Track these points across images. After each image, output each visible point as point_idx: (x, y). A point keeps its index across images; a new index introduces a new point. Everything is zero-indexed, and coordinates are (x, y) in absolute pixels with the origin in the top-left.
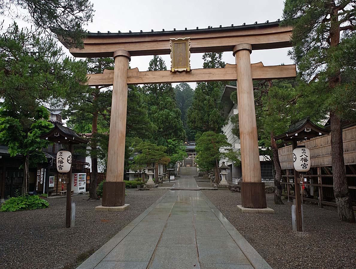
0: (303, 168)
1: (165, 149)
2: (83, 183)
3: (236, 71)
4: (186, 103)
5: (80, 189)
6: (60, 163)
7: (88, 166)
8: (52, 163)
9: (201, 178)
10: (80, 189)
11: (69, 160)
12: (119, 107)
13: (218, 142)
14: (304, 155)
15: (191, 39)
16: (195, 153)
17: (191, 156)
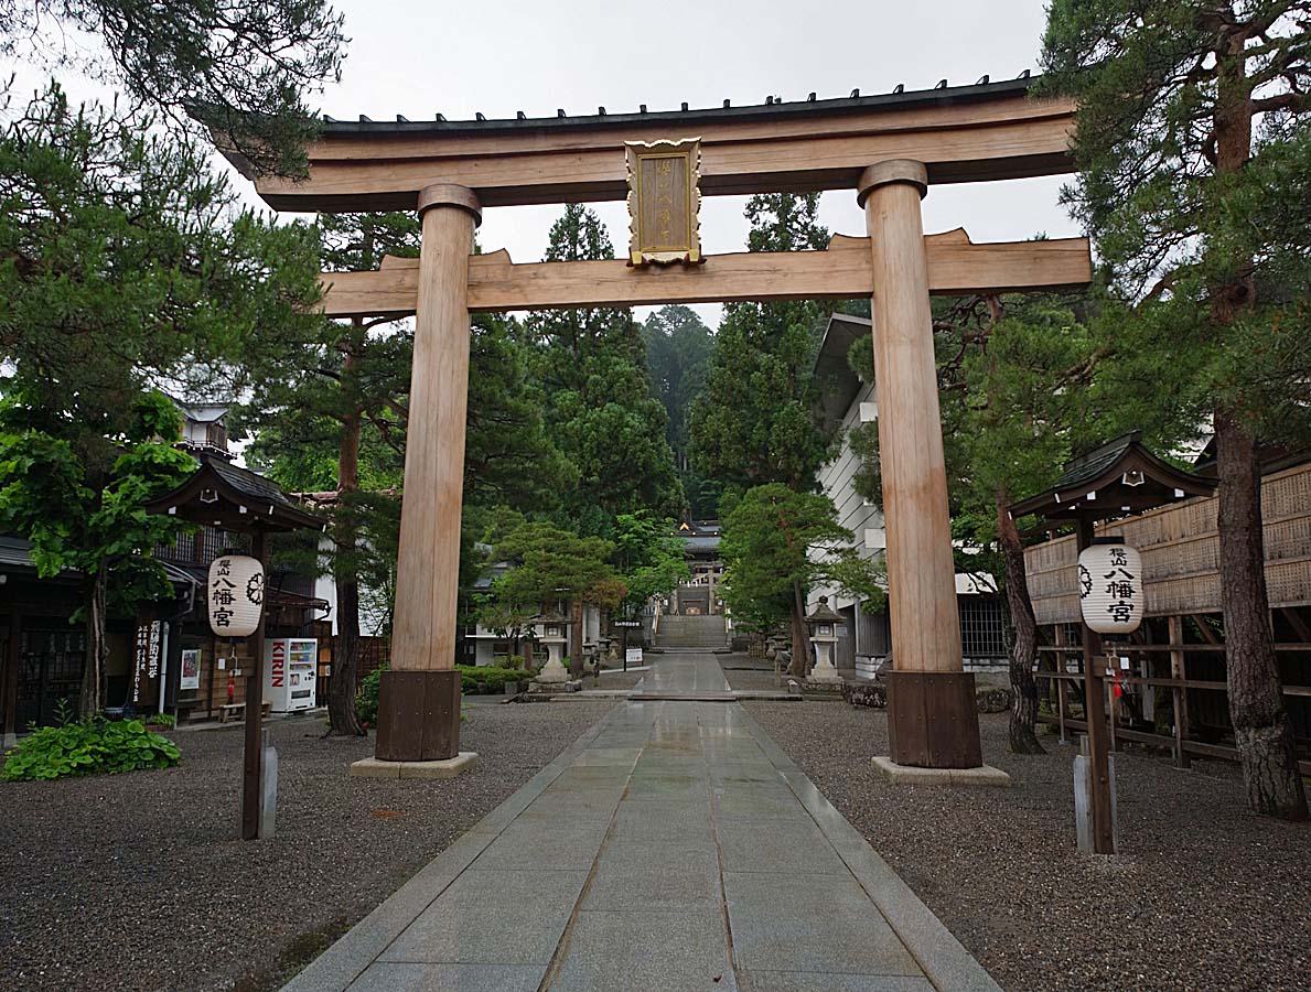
0: (1116, 620)
1: (608, 549)
2: (304, 674)
3: (870, 260)
4: (685, 380)
5: (295, 695)
6: (220, 601)
7: (325, 613)
8: (191, 602)
9: (740, 656)
10: (295, 695)
11: (254, 590)
12: (438, 394)
13: (802, 525)
14: (1118, 573)
15: (703, 145)
16: (719, 563)
17: (704, 576)
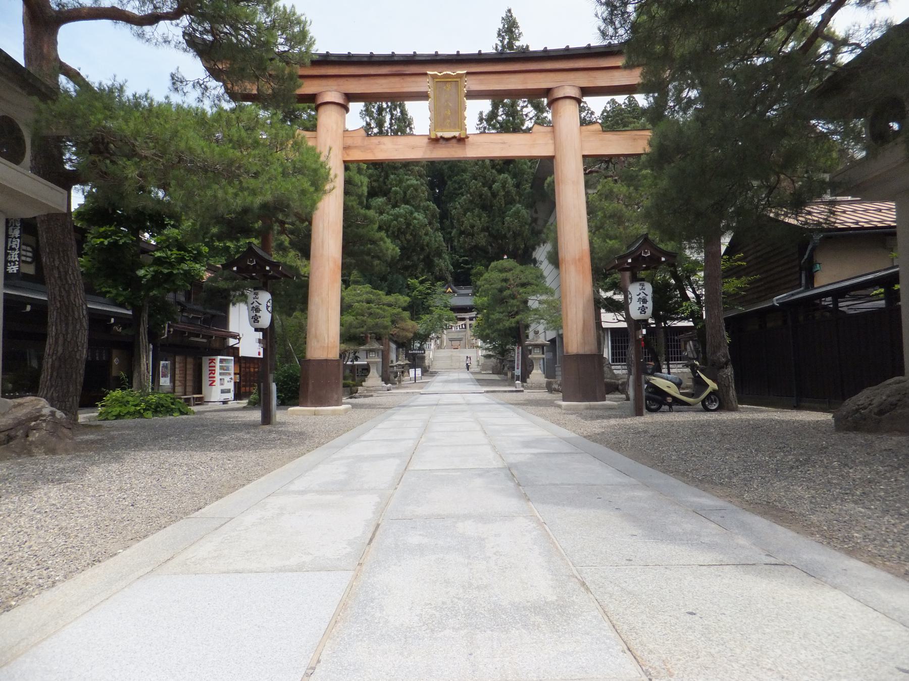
1: (405, 301)
2: (227, 378)
3: (553, 132)
5: (223, 392)
7: (237, 341)
10: (223, 392)
13: (523, 285)
16: (473, 314)
17: (463, 322)
